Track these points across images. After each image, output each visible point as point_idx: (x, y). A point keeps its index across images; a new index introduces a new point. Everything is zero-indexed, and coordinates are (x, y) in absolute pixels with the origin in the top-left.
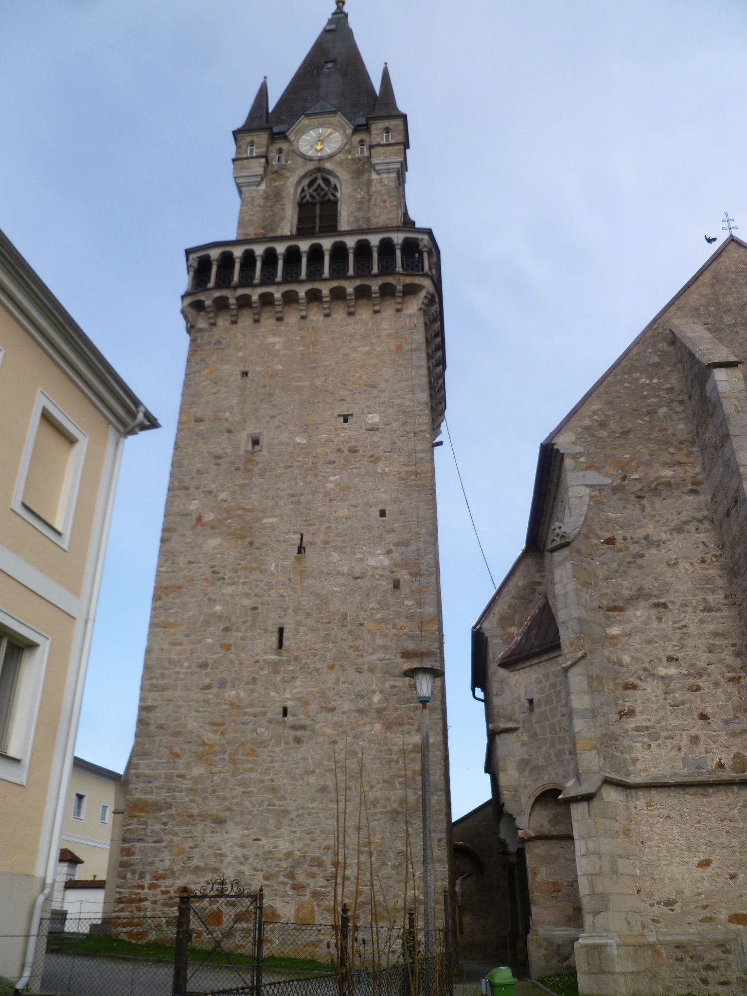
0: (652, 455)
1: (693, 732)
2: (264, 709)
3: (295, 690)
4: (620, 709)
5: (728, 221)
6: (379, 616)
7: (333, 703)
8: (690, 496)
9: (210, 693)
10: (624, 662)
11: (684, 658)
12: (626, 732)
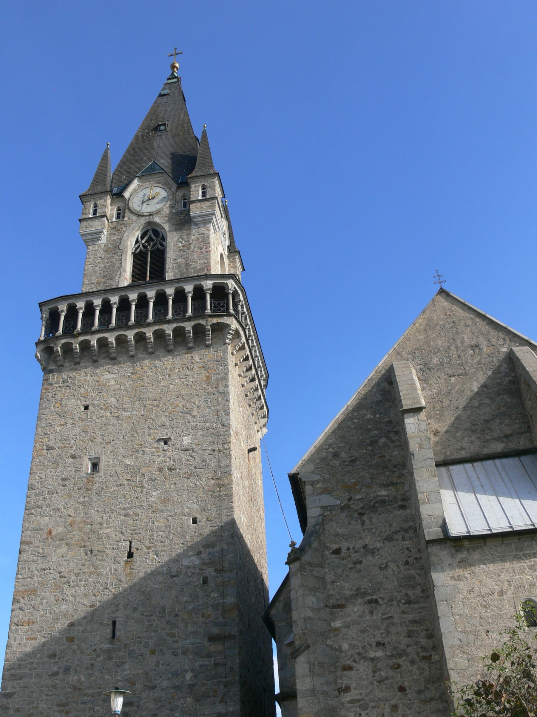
0: (373, 478)
1: (393, 702)
2: (99, 690)
3: (125, 673)
4: (338, 686)
5: (438, 276)
6: (190, 607)
7: (154, 682)
8: (399, 510)
9: (57, 679)
10: (344, 649)
11: (389, 643)
12: (343, 704)
